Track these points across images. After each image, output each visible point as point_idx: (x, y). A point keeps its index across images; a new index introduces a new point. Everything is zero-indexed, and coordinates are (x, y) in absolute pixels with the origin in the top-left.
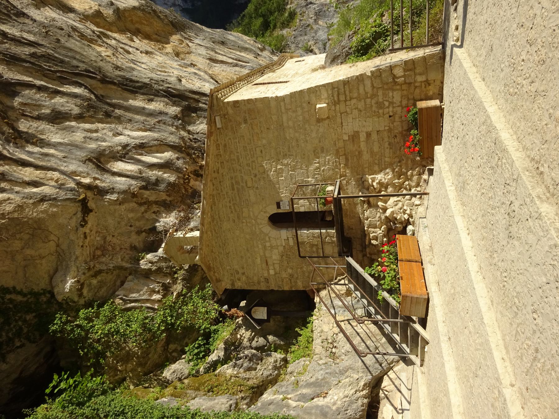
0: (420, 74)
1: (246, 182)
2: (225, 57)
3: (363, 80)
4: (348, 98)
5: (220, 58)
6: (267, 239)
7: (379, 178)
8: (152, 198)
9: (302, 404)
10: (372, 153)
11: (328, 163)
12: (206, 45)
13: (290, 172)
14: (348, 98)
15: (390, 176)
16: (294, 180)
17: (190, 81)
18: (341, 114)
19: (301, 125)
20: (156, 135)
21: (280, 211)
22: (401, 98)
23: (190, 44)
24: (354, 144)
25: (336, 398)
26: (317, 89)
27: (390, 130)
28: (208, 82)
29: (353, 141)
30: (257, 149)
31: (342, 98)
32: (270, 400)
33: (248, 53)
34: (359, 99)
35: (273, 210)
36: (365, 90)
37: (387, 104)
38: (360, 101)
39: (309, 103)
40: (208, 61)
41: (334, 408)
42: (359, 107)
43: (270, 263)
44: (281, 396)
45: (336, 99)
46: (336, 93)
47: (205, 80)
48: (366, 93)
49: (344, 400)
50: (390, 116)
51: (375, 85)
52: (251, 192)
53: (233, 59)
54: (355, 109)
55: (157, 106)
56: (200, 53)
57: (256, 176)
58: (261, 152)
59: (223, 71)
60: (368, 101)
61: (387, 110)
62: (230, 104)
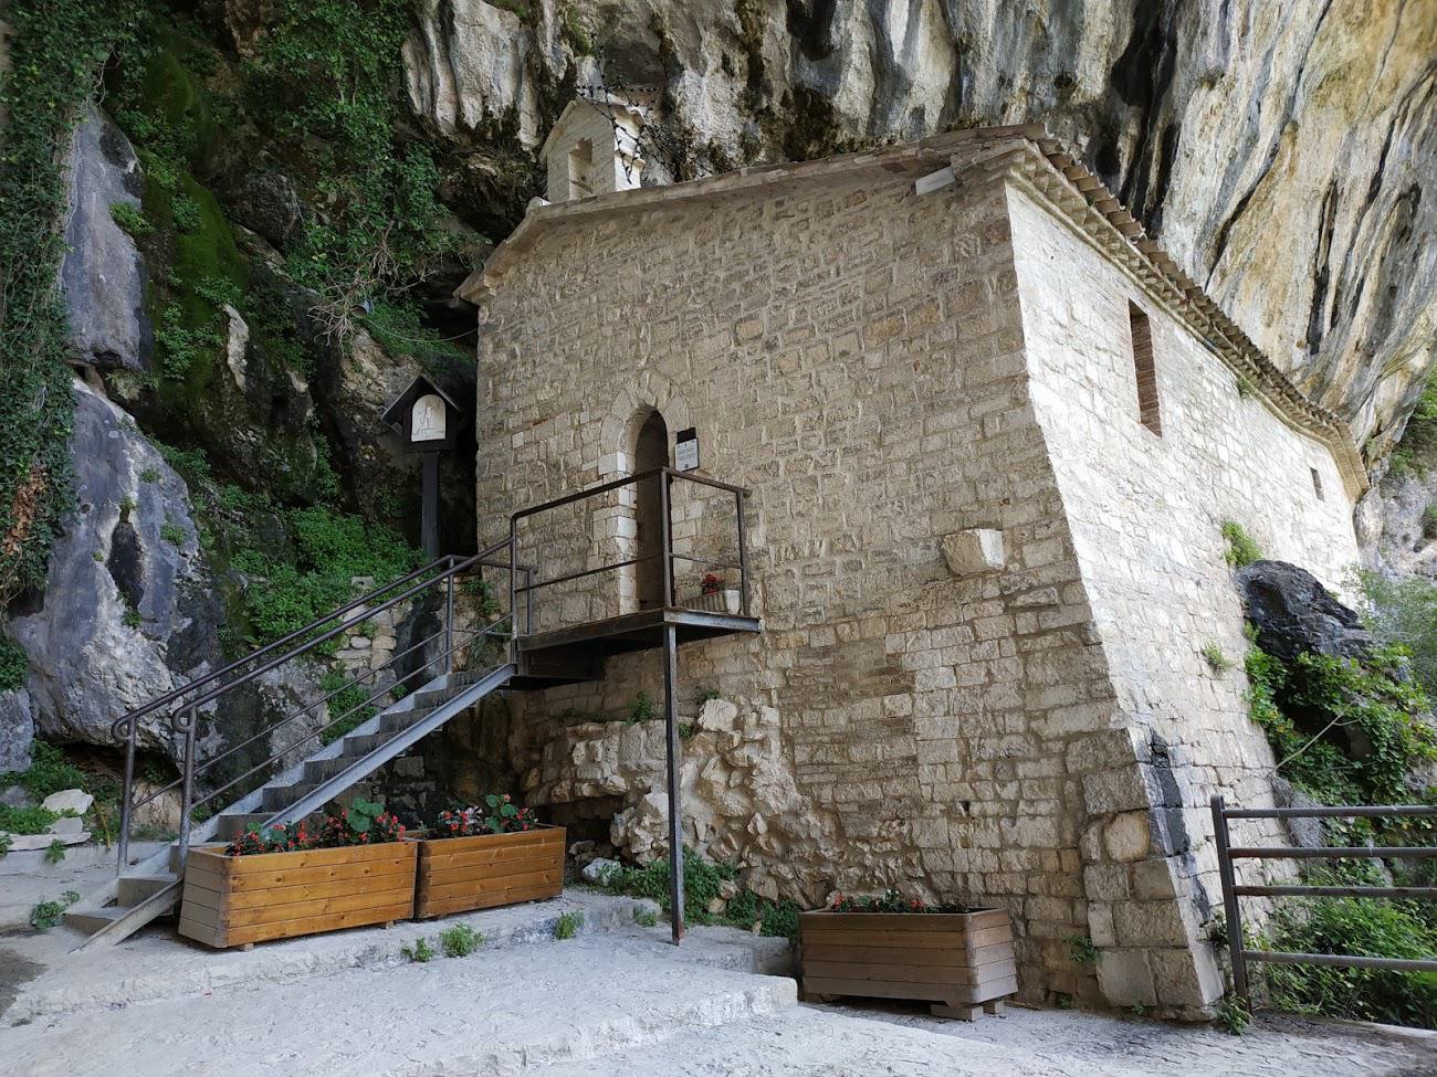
0: (1115, 926)
1: (751, 318)
2: (1345, 244)
3: (1092, 698)
4: (1028, 645)
5: (1343, 229)
6: (598, 414)
7: (765, 766)
8: (768, 49)
9: (106, 556)
10: (844, 741)
11: (812, 588)
12: (1385, 175)
13: (782, 463)
14: (1028, 645)
15: (773, 803)
16: (759, 476)
17: (1215, 121)
18: (971, 623)
19: (929, 481)
20: (988, 24)
21: (672, 441)
22: (1034, 848)
23: (1384, 120)
24: (871, 674)
25: (119, 652)
26: (1055, 526)
27: (919, 805)
28: (1226, 188)
29: (882, 672)
30: (853, 335)
31: (1026, 623)
32: (127, 465)
33: (1374, 320)
34: (1026, 687)
35: (673, 427)
36: (1053, 708)
37: (1010, 791)
38: (1021, 692)
39: (1006, 501)
40: (1323, 189)
41: (89, 649)
42: (995, 690)
43: (537, 432)
44: (134, 496)
45: (1021, 600)
46: (1043, 600)
47: (1231, 174)
48: (1045, 714)
49: (110, 677)
50: (967, 805)
51: (1075, 748)
52: (724, 339)
53: (1343, 271)
54: (989, 673)
55: (1100, 13)
56: (1354, 159)
57: (770, 347)
58: (844, 354)
59: (1294, 242)
60: (1017, 723)
61: (989, 794)
62: (997, 212)
